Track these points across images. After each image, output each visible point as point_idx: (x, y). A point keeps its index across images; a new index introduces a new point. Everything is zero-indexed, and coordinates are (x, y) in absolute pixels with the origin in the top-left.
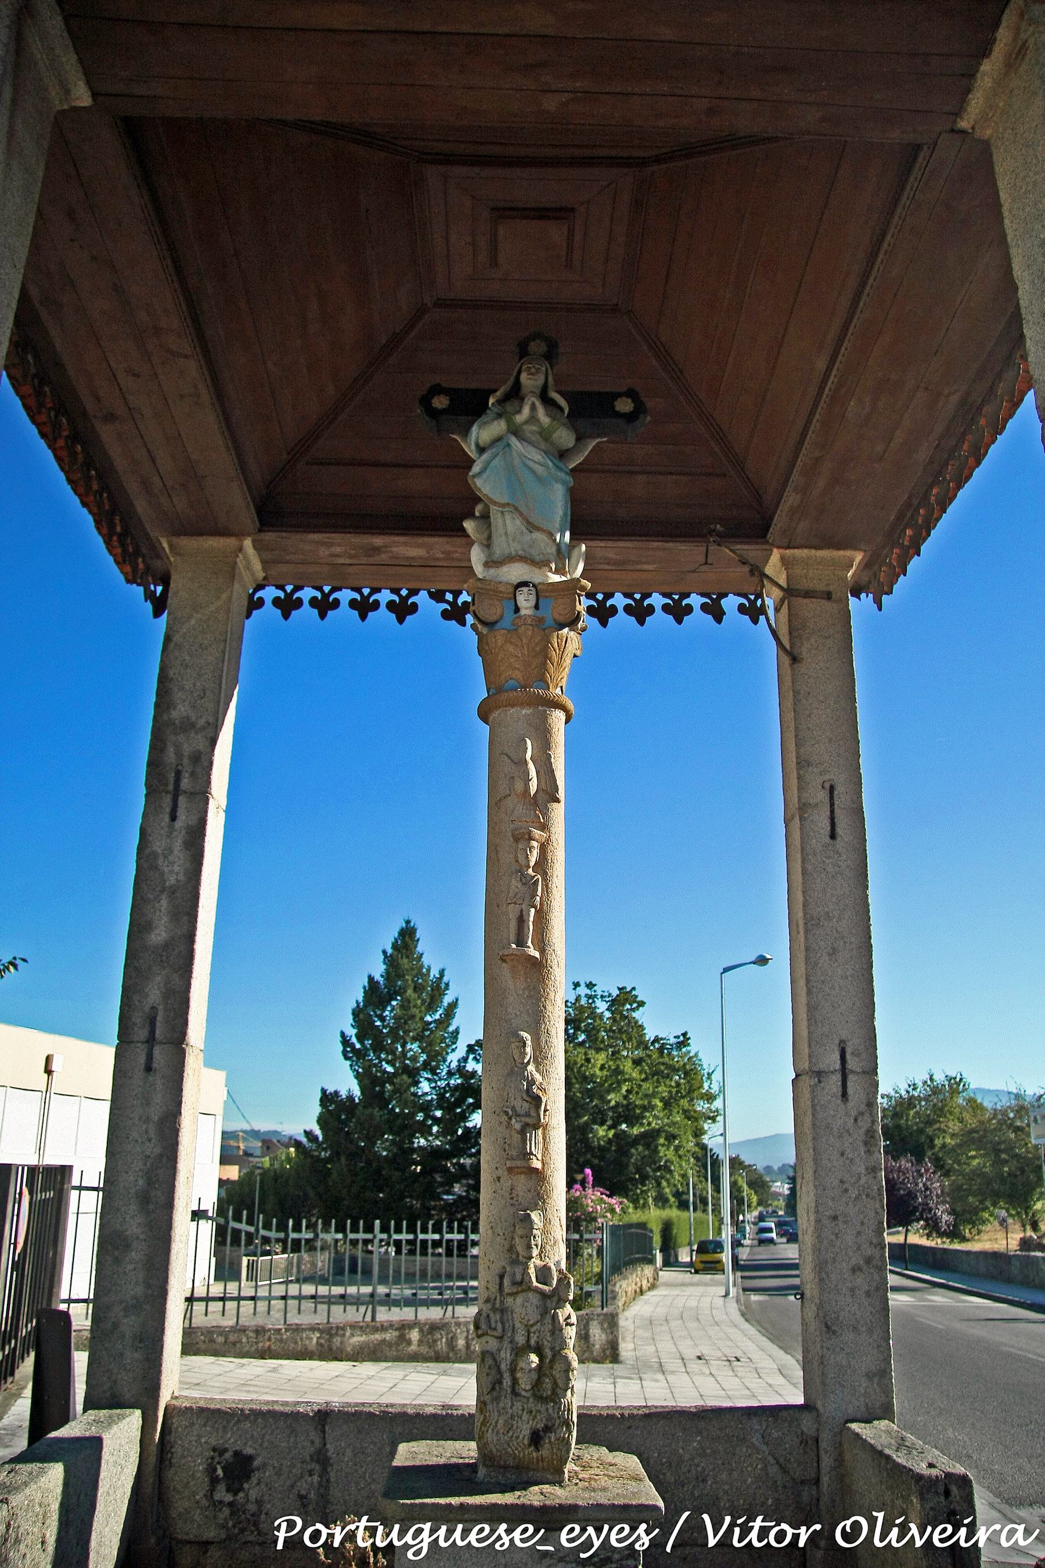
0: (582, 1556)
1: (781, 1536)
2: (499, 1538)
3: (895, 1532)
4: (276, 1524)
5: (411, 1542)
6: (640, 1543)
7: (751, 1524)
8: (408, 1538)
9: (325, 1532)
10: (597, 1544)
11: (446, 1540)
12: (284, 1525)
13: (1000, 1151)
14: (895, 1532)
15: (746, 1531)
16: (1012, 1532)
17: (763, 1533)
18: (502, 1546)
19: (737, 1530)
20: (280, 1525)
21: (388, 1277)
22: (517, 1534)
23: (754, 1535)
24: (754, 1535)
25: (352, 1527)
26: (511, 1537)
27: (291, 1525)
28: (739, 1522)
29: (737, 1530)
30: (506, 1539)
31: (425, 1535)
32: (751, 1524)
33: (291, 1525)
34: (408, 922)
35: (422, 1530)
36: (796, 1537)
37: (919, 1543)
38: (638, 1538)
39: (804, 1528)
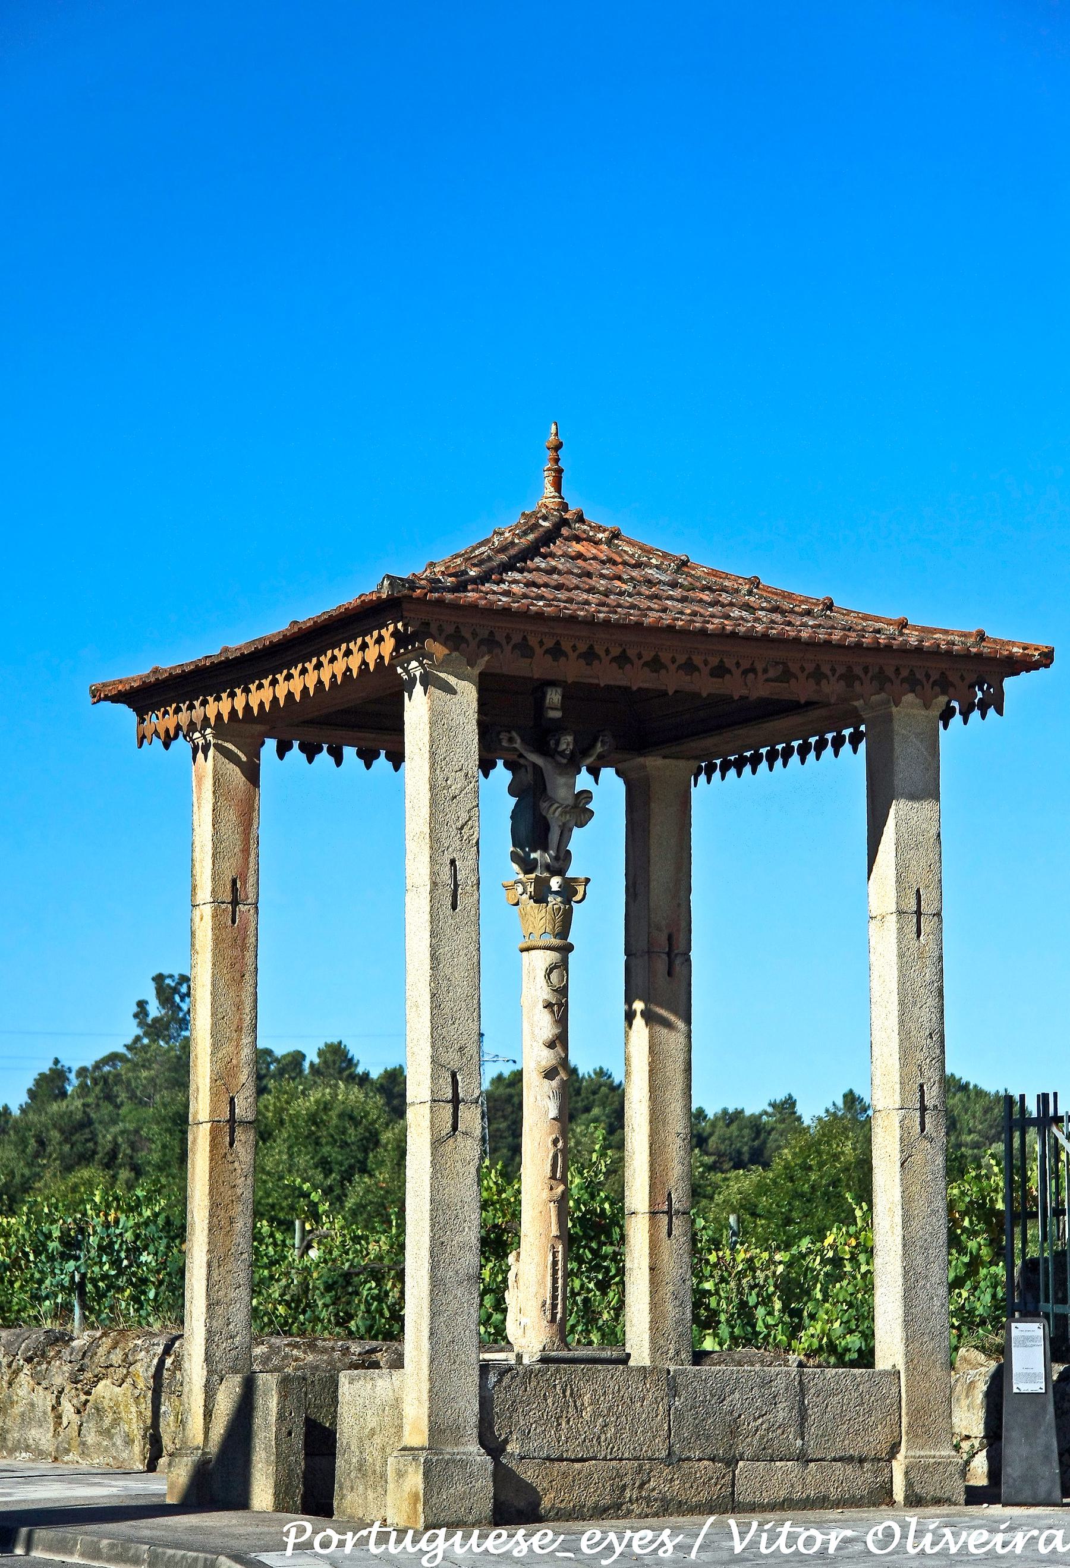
0: (604, 1562)
1: (809, 1541)
2: (663, 1544)
3: (928, 1538)
4: (285, 1529)
5: (425, 1549)
6: (519, 1548)
7: (778, 1530)
8: (423, 1544)
9: (819, 1538)
10: (619, 1550)
11: (462, 1546)
12: (293, 1531)
13: (379, 1279)
14: (928, 1538)
15: (773, 1539)
16: (1049, 1541)
17: (792, 1539)
18: (665, 1552)
19: (765, 1536)
20: (288, 1531)
21: (687, 1206)
22: (535, 1540)
23: (782, 1541)
24: (782, 1541)
25: (364, 1533)
26: (529, 1543)
27: (301, 1531)
28: (767, 1527)
29: (765, 1536)
30: (524, 1546)
31: (440, 1540)
32: (778, 1530)
33: (301, 1531)
34: (57, 1061)
35: (436, 1536)
36: (826, 1543)
37: (953, 1550)
38: (663, 1544)
39: (350, 1534)
